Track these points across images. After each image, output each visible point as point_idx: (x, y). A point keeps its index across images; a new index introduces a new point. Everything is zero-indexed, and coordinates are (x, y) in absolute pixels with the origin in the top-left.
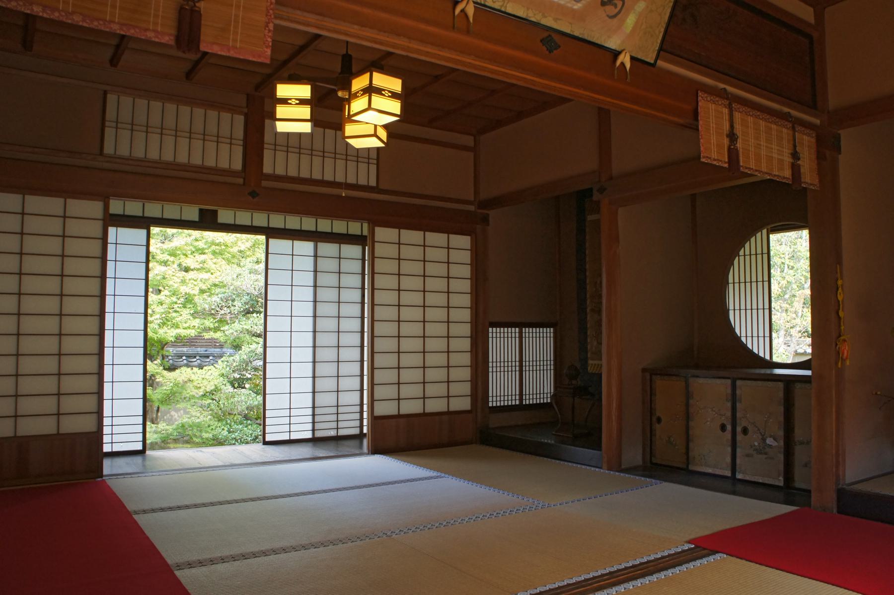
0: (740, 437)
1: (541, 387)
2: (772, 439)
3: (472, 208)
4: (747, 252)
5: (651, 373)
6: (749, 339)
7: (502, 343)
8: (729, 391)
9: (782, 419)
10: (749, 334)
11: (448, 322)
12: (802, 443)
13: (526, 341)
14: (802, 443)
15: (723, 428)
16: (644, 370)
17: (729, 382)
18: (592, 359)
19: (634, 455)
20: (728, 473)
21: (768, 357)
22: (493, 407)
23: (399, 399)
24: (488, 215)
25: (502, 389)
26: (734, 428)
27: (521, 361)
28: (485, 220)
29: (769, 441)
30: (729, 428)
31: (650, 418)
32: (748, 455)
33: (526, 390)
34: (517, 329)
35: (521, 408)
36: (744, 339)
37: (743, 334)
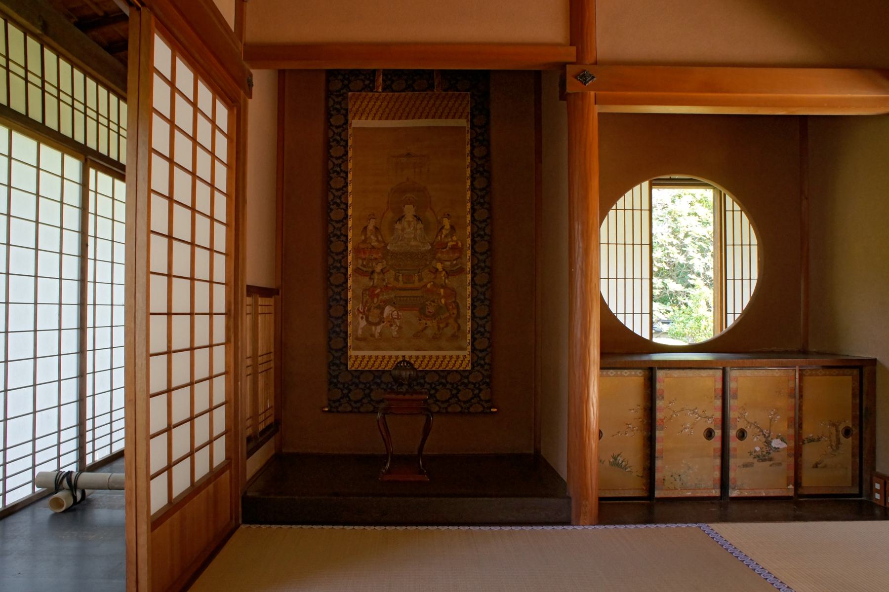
0: (734, 443)
2: (779, 440)
4: (629, 206)
6: (629, 317)
8: (719, 385)
10: (629, 310)
12: (811, 440)
14: (811, 440)
15: (709, 434)
20: (716, 493)
21: (646, 336)
29: (776, 443)
30: (718, 433)
32: (745, 465)
36: (621, 318)
37: (621, 310)
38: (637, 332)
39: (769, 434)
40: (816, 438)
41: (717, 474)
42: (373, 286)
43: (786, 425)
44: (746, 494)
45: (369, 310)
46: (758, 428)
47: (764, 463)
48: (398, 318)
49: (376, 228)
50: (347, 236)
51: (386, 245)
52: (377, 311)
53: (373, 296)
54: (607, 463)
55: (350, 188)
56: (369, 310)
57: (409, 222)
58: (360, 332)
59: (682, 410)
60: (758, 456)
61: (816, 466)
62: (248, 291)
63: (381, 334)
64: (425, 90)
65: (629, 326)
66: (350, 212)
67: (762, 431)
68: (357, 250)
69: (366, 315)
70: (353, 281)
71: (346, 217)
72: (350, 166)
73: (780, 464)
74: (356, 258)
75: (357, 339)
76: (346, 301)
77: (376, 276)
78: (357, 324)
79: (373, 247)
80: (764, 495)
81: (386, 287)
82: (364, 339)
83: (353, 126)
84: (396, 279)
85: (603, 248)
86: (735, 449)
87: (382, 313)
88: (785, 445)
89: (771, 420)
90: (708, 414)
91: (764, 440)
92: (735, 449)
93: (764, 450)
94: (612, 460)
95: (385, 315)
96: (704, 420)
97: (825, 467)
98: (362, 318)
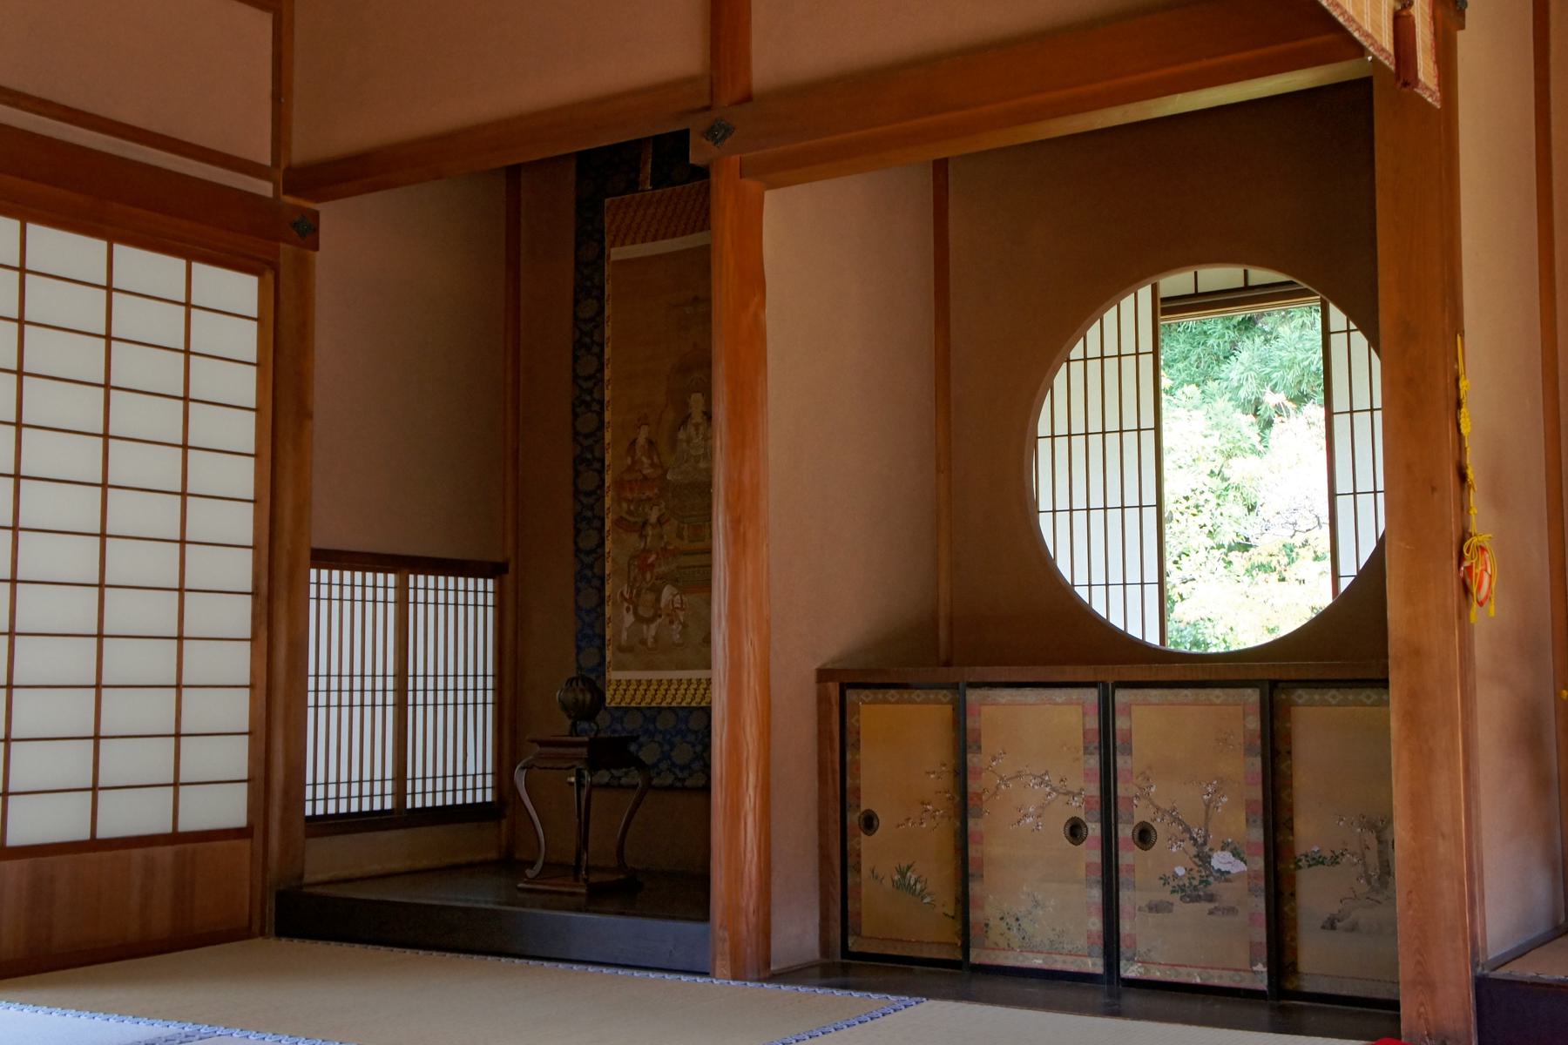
0: (1128, 856)
1: (457, 759)
2: (1227, 855)
3: (265, 188)
4: (1094, 350)
5: (844, 685)
7: (347, 618)
8: (1093, 723)
9: (1257, 793)
10: (1098, 578)
11: (183, 542)
12: (1318, 861)
13: (419, 616)
14: (1318, 861)
15: (1075, 831)
16: (824, 675)
17: (1092, 695)
18: (621, 667)
19: (797, 932)
20: (1095, 965)
21: (1153, 639)
22: (314, 817)
23: (178, 735)
24: (316, 215)
25: (345, 764)
26: (1108, 830)
27: (401, 675)
28: (307, 232)
30: (1094, 829)
31: (843, 818)
32: (1154, 908)
33: (415, 767)
34: (391, 577)
35: (400, 818)
36: (1082, 593)
38: (1134, 631)
39: (1206, 837)
40: (1328, 854)
41: (1096, 924)
42: (644, 550)
43: (1243, 817)
44: (1157, 974)
45: (638, 594)
46: (1181, 822)
47: (1197, 905)
48: (682, 609)
49: (650, 442)
50: (602, 461)
51: (666, 472)
52: (650, 597)
53: (645, 567)
54: (887, 883)
55: (607, 373)
56: (638, 594)
57: (697, 426)
58: (624, 635)
59: (1019, 775)
60: (1182, 888)
61: (1331, 924)
62: (313, 557)
63: (656, 639)
64: (688, 182)
65: (1099, 607)
66: (607, 416)
67: (1187, 830)
68: (620, 485)
69: (634, 603)
70: (614, 542)
71: (601, 425)
72: (608, 332)
73: (1231, 910)
74: (618, 500)
75: (621, 649)
76: (602, 579)
77: (649, 531)
78: (620, 622)
79: (645, 478)
80: (1198, 981)
81: (664, 549)
82: (629, 649)
83: (613, 258)
84: (680, 536)
85: (1044, 446)
86: (1131, 869)
87: (658, 600)
88: (1242, 867)
89: (1208, 806)
90: (1073, 785)
91: (1194, 851)
92: (1131, 869)
93: (1196, 875)
94: (896, 877)
95: (662, 605)
96: (1066, 798)
97: (1354, 928)
98: (628, 609)
